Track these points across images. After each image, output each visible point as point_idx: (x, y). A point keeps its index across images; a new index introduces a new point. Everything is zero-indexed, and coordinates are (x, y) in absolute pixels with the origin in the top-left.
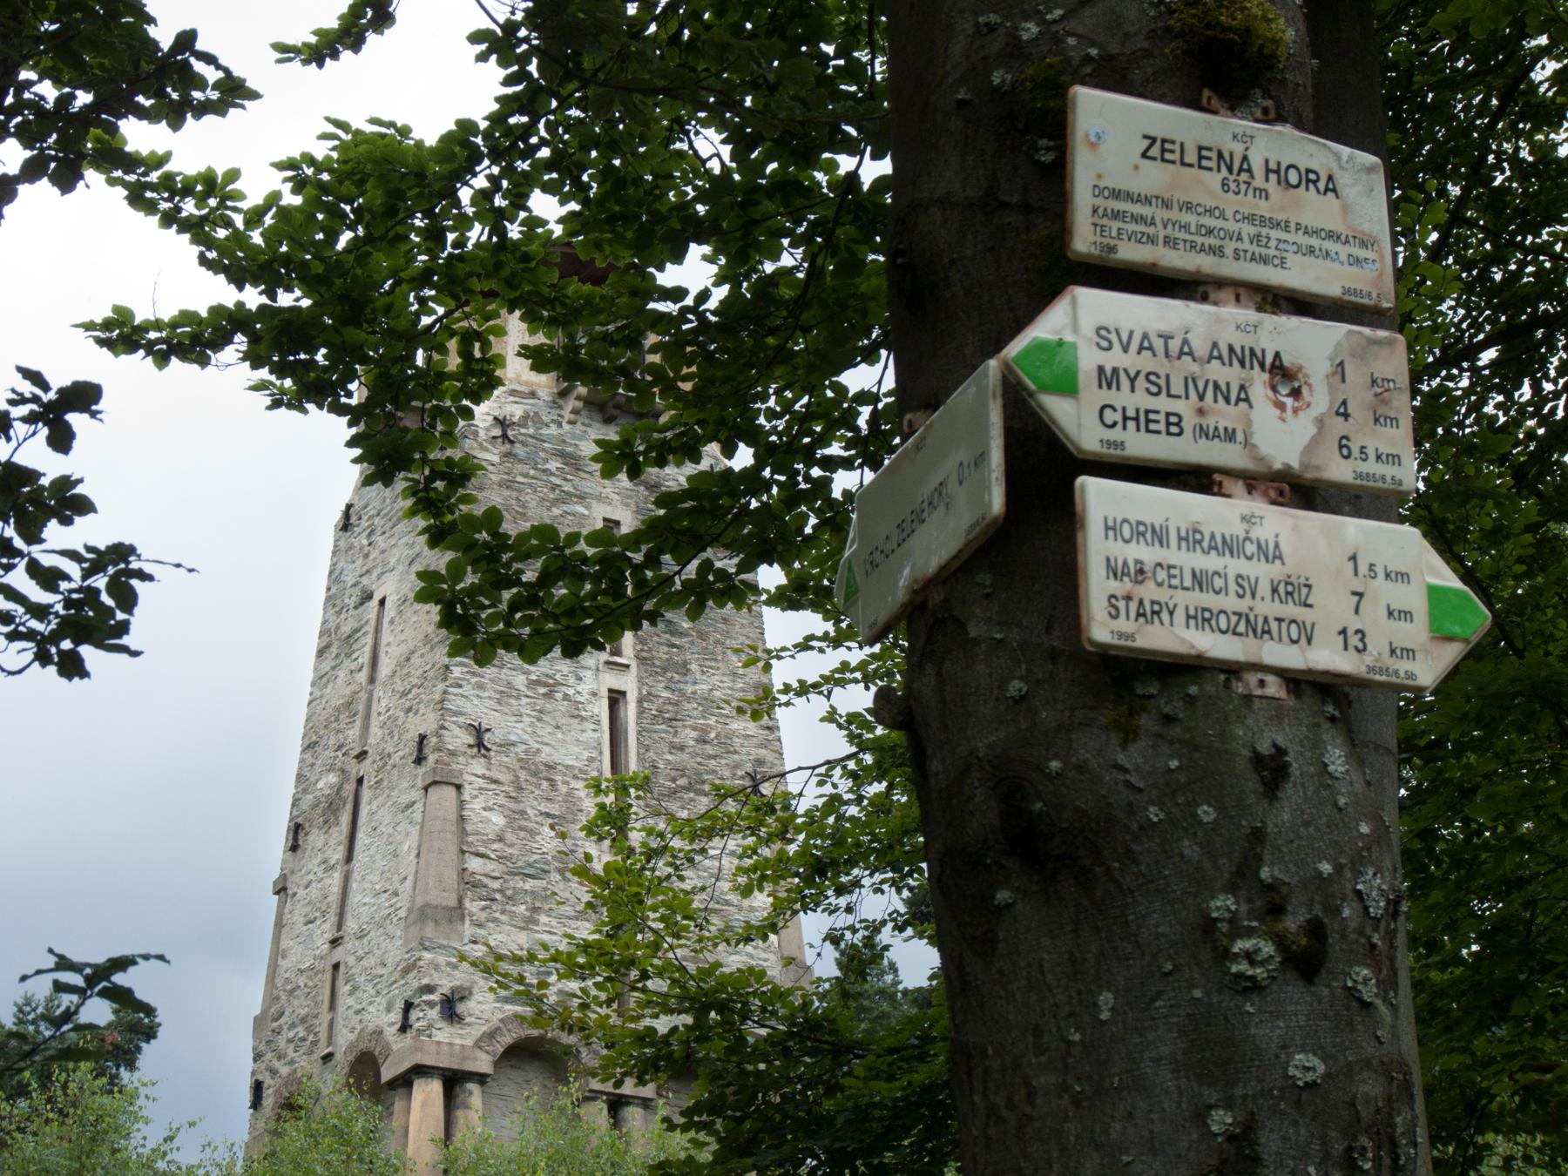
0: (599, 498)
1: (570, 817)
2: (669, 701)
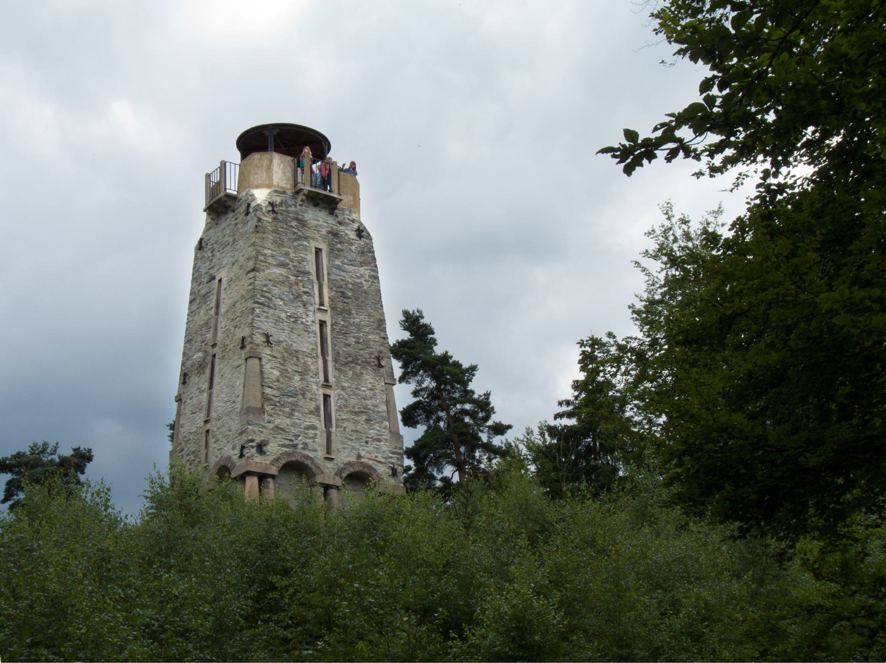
0: (313, 239)
2: (343, 326)
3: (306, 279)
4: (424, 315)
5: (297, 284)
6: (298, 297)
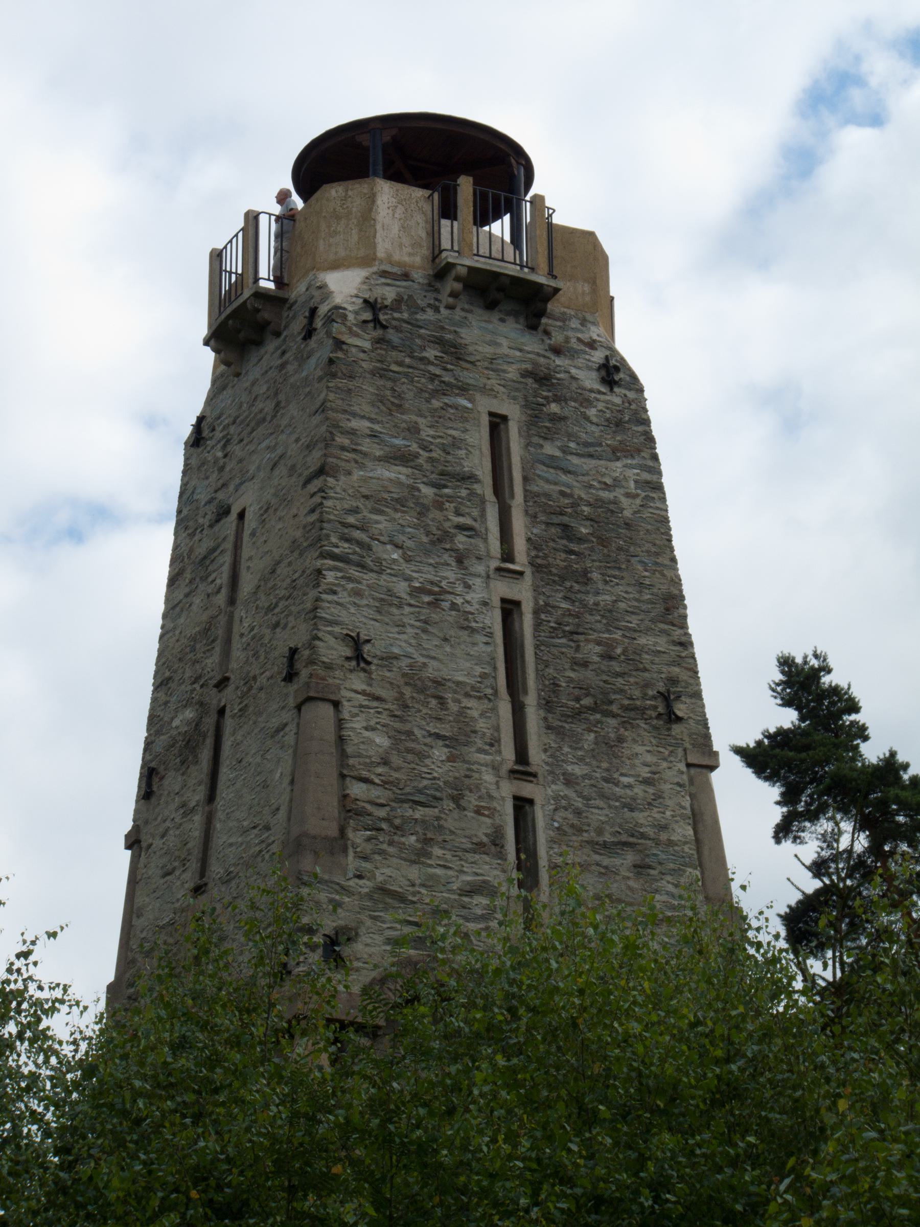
0: (485, 391)
1: (463, 738)
2: (568, 613)
3: (464, 493)
4: (832, 662)
5: (439, 506)
6: (441, 539)
